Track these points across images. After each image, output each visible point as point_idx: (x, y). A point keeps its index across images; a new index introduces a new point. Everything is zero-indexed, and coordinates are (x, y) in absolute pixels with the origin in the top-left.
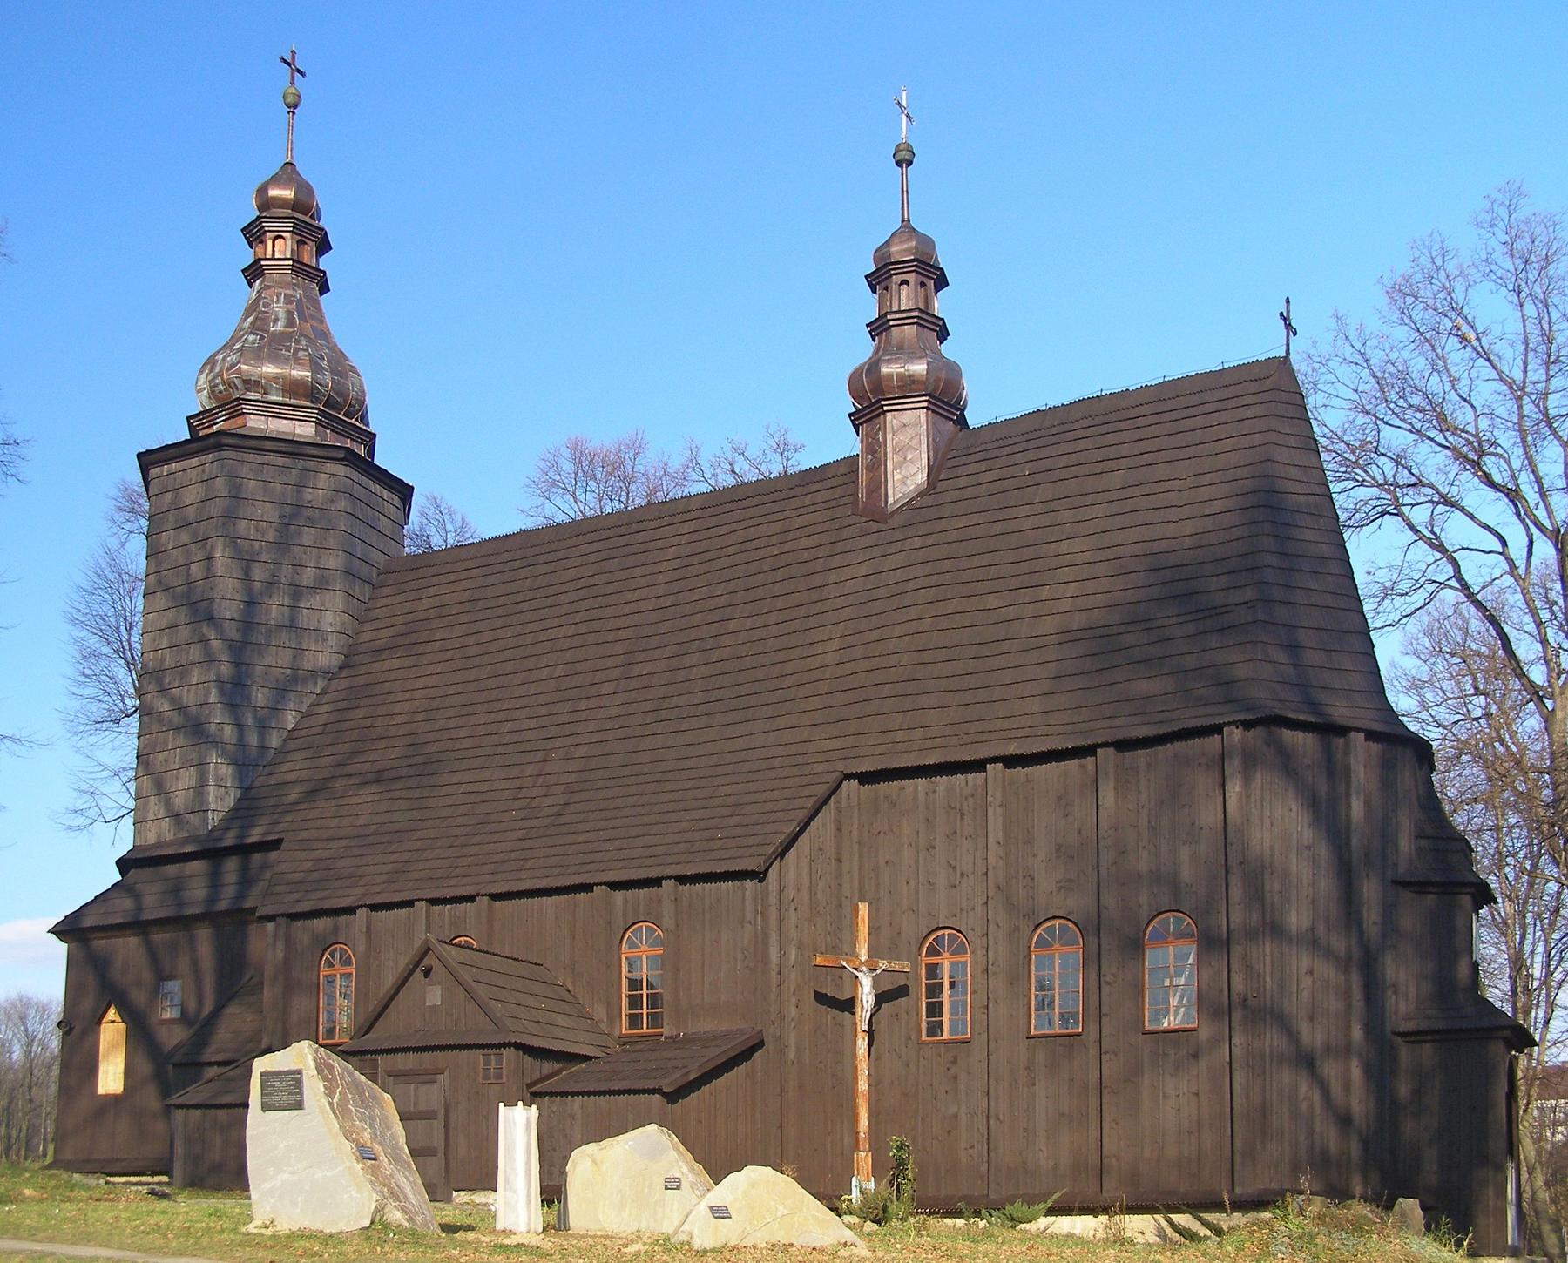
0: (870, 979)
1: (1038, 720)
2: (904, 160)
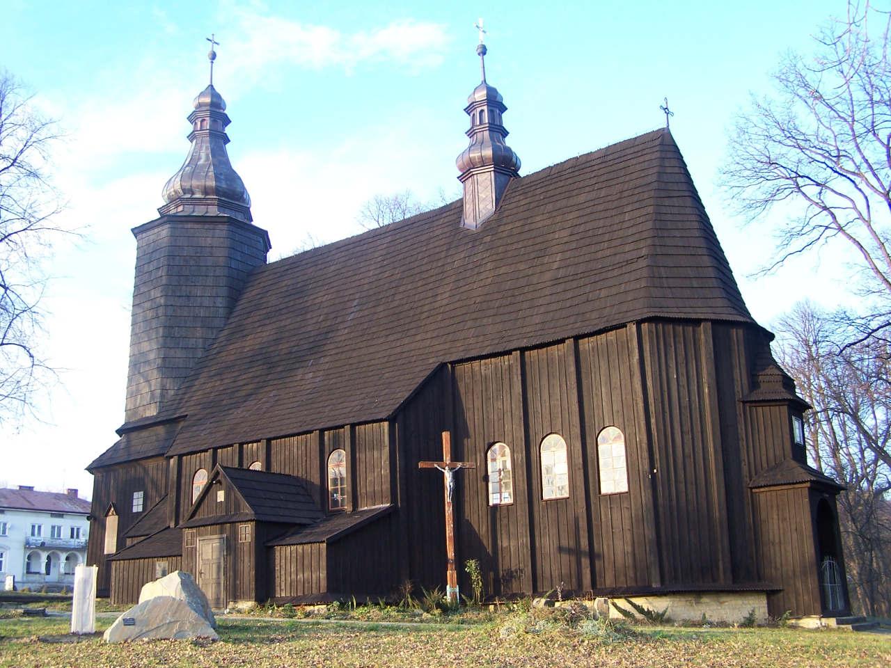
0: (451, 473)
1: (539, 327)
2: (483, 51)
